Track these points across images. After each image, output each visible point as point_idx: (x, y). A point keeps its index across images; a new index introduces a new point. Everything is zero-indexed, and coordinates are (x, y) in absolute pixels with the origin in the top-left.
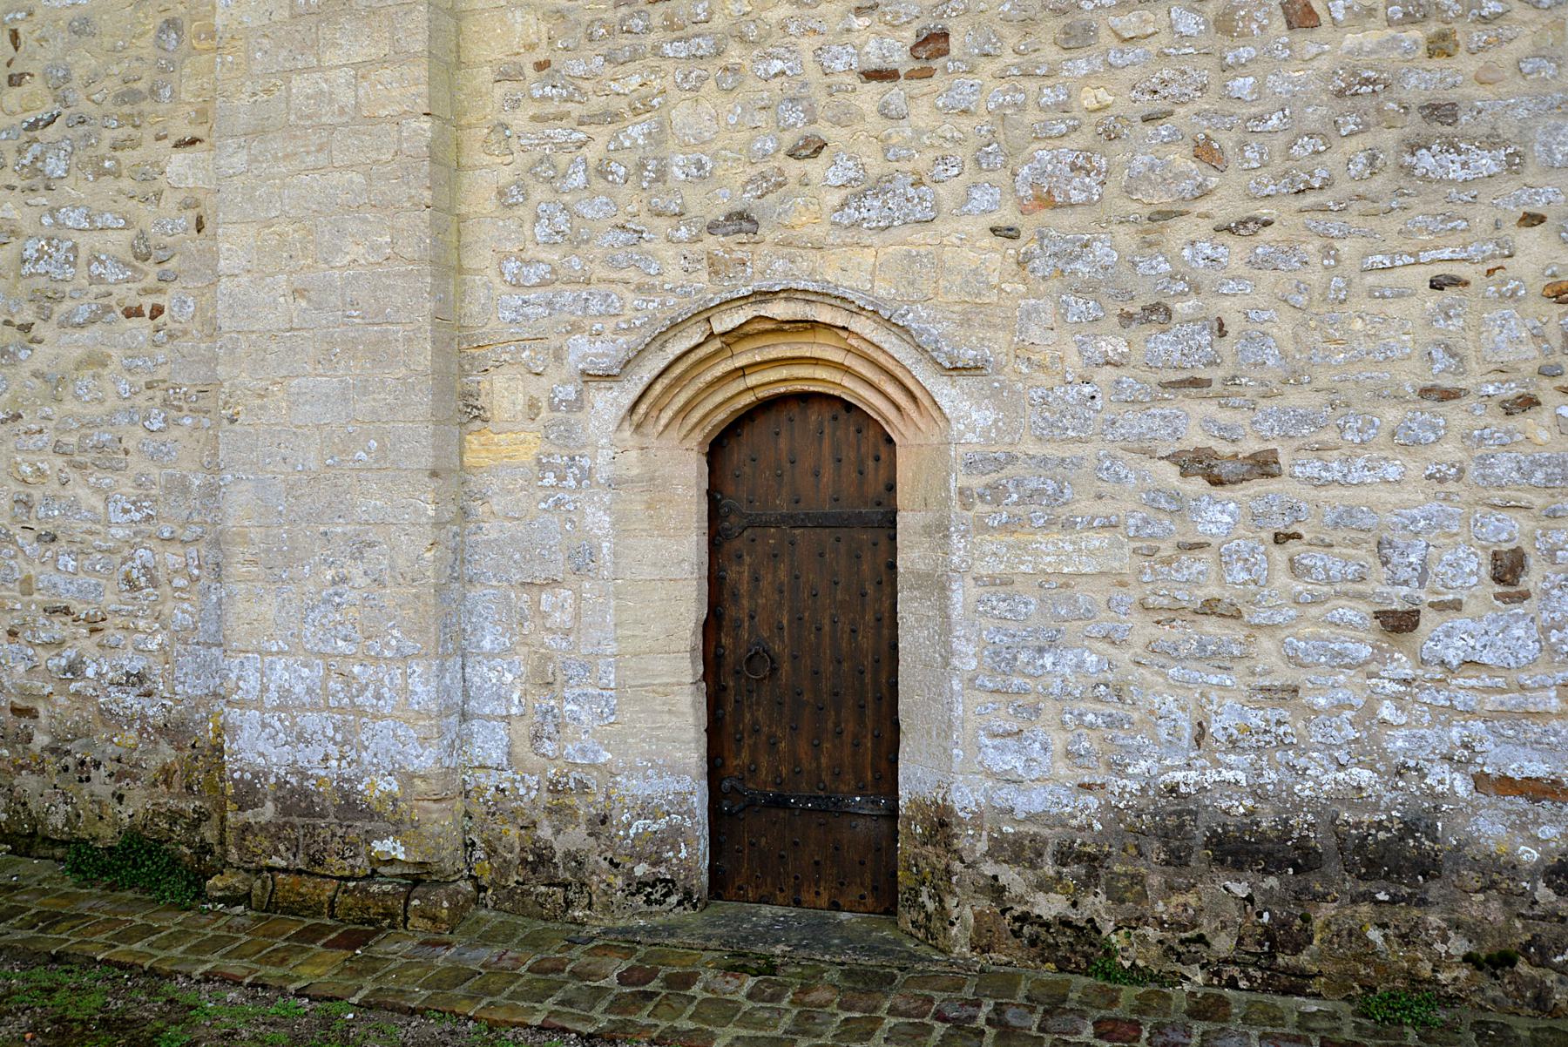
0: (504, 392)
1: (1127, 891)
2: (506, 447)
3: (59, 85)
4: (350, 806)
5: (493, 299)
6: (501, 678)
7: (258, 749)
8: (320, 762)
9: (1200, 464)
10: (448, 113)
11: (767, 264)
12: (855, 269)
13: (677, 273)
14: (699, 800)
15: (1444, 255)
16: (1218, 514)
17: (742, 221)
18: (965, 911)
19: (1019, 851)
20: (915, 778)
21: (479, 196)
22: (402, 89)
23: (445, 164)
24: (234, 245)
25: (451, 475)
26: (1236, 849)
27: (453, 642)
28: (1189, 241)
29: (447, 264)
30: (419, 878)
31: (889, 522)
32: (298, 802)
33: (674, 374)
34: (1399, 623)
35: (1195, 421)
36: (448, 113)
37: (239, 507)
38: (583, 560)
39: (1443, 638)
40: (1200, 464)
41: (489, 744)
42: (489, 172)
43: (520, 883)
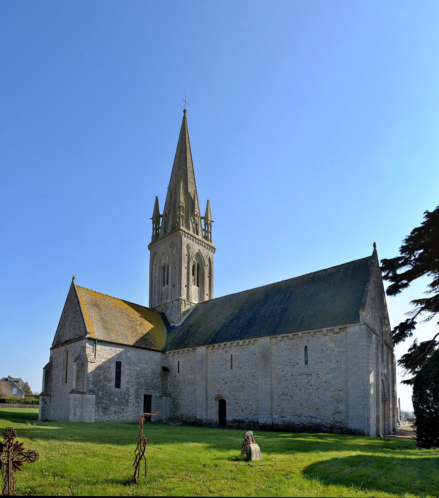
0: (209, 399)
1: (233, 424)
2: (209, 402)
3: (190, 381)
4: (202, 420)
5: (209, 394)
6: (209, 413)
7: (198, 417)
8: (201, 418)
9: (235, 403)
10: (207, 385)
11: (220, 393)
12: (223, 393)
13: (216, 393)
14: (218, 420)
15: (244, 394)
16: (236, 405)
17: (219, 391)
18: (227, 425)
19: (229, 422)
20: (227, 419)
21: (208, 389)
22: (205, 384)
23: (207, 387)
24: (197, 391)
25: (207, 403)
26: (237, 421)
27: (207, 412)
28: (235, 392)
29: (207, 392)
30: (205, 423)
31: (121, 373)
32: (200, 420)
33: (217, 398)
34: (243, 410)
35: (235, 401)
36: (207, 385)
37: (197, 405)
38: (212, 407)
39: (244, 411)
40: (235, 403)
41: (208, 417)
42: (209, 388)
43: (146, 308)
